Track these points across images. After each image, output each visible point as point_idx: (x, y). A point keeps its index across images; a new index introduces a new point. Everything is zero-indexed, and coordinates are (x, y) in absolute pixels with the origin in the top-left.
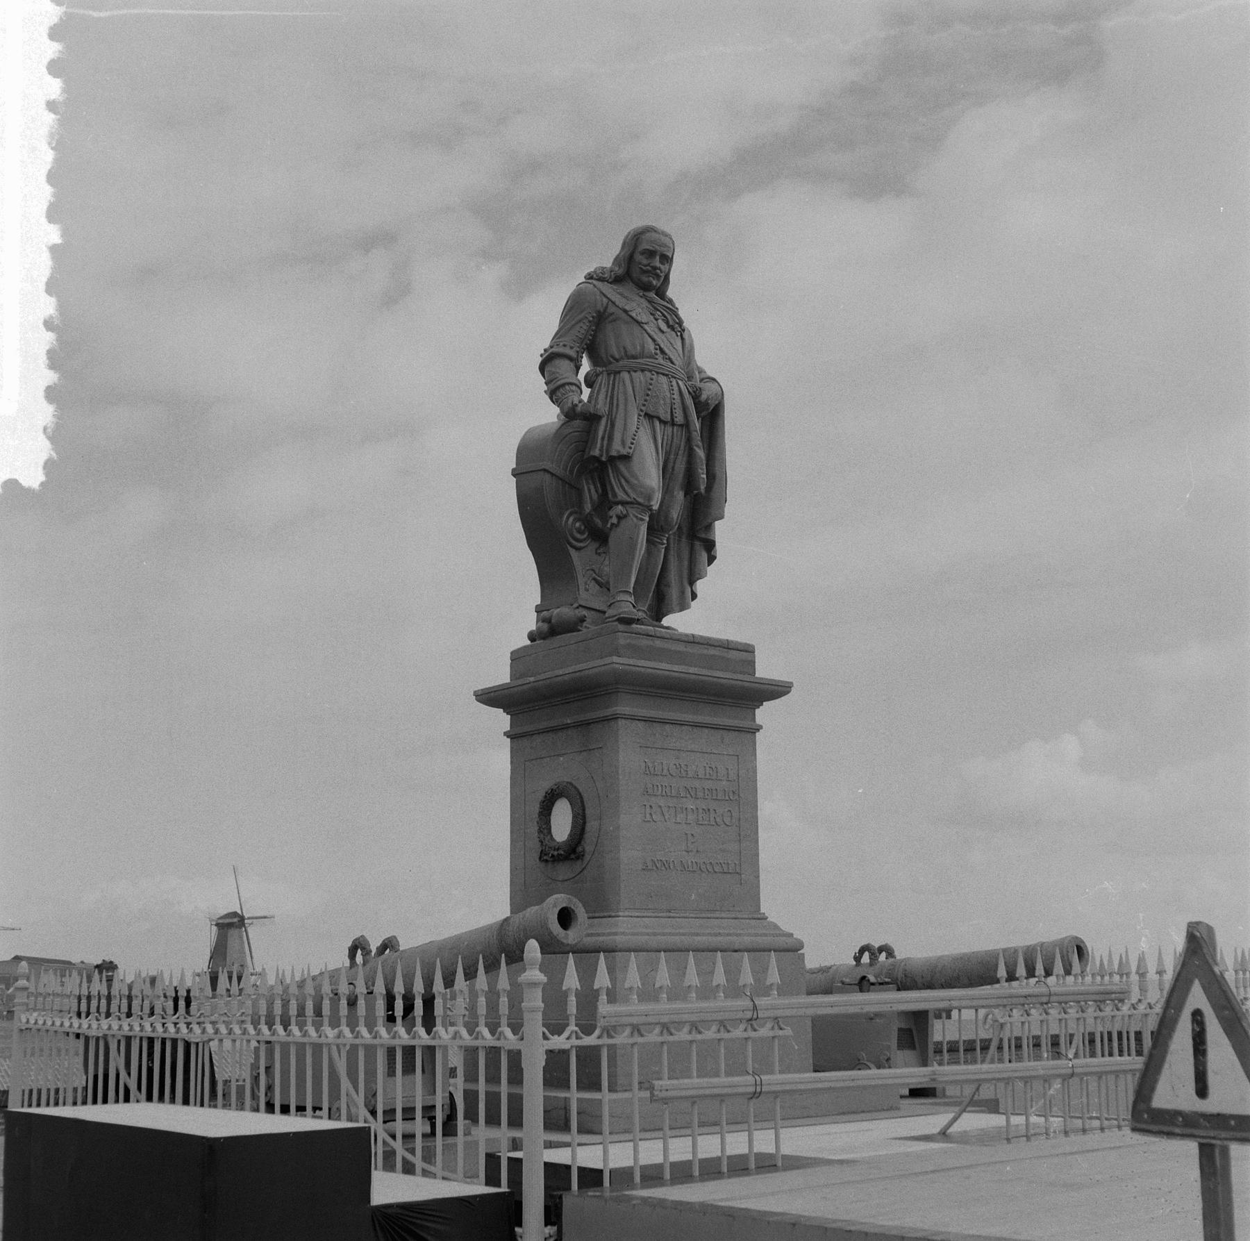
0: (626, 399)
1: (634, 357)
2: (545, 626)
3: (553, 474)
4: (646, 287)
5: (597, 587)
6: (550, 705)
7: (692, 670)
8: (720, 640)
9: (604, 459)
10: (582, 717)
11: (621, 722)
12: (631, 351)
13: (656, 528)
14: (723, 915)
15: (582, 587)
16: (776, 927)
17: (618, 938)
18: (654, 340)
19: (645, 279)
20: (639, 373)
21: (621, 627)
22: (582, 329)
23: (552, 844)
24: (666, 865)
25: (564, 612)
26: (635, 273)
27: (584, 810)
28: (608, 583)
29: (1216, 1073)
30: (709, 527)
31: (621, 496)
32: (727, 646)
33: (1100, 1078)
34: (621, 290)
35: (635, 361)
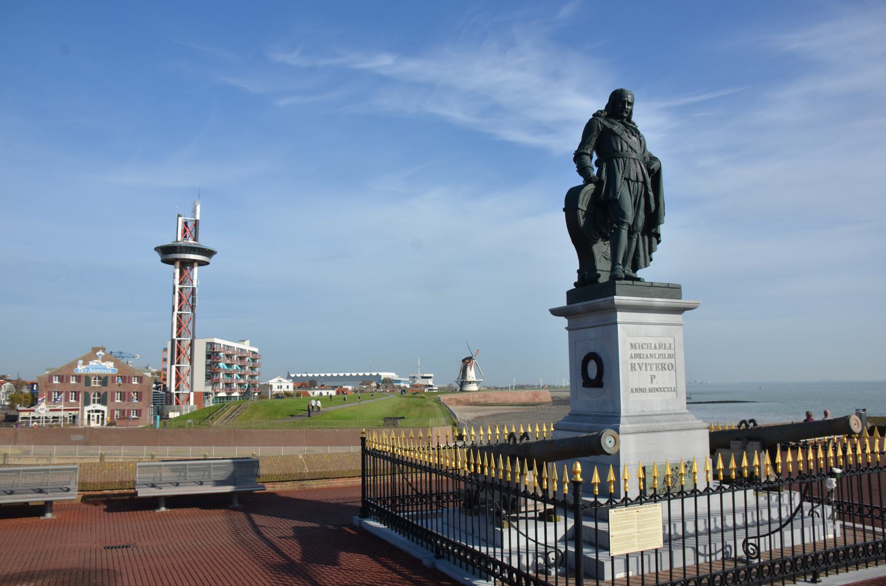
29: (826, 414)
32: (589, 387)
33: (643, 492)
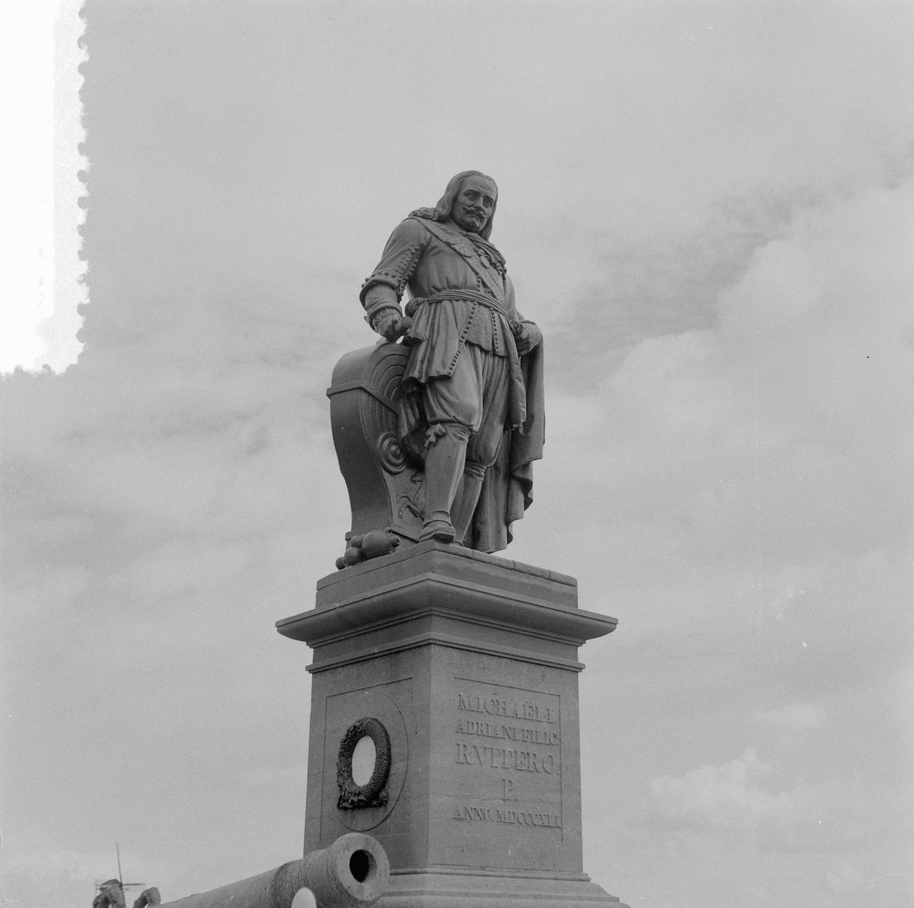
0: (447, 325)
1: (456, 287)
2: (355, 551)
3: (369, 394)
4: (468, 228)
5: (411, 515)
6: (357, 634)
7: (513, 595)
8: (543, 571)
9: (423, 381)
10: (390, 645)
11: (434, 649)
12: (453, 281)
13: (473, 460)
14: (543, 875)
15: (395, 513)
16: (599, 889)
17: (425, 898)
18: (477, 273)
19: (468, 219)
20: (461, 303)
21: (438, 545)
22: (404, 261)
23: (353, 789)
24: (480, 814)
25: (378, 535)
26: (459, 213)
27: (389, 749)
28: (423, 512)
30: (526, 466)
31: (440, 414)
32: (549, 577)
34: (444, 227)
35: (455, 291)
